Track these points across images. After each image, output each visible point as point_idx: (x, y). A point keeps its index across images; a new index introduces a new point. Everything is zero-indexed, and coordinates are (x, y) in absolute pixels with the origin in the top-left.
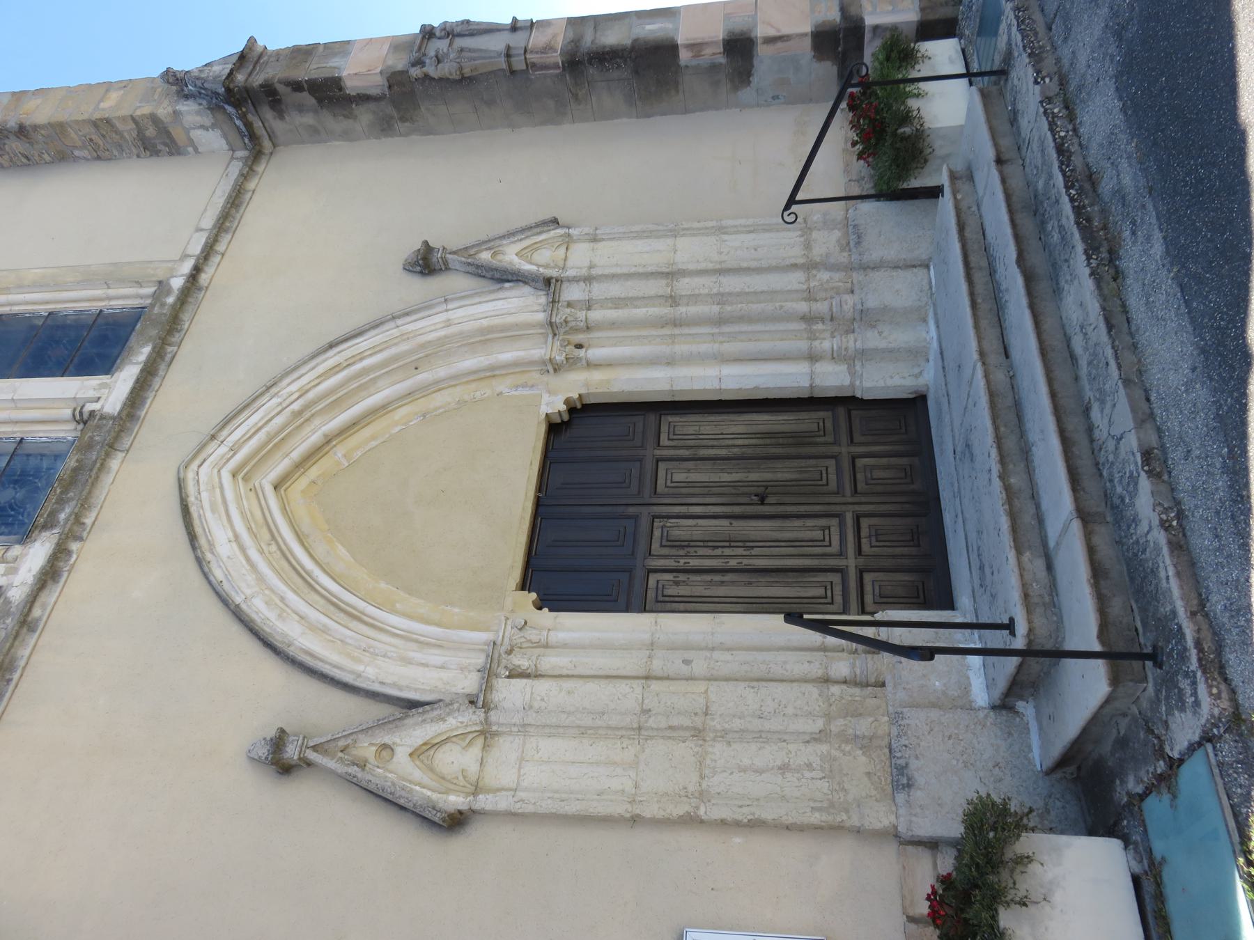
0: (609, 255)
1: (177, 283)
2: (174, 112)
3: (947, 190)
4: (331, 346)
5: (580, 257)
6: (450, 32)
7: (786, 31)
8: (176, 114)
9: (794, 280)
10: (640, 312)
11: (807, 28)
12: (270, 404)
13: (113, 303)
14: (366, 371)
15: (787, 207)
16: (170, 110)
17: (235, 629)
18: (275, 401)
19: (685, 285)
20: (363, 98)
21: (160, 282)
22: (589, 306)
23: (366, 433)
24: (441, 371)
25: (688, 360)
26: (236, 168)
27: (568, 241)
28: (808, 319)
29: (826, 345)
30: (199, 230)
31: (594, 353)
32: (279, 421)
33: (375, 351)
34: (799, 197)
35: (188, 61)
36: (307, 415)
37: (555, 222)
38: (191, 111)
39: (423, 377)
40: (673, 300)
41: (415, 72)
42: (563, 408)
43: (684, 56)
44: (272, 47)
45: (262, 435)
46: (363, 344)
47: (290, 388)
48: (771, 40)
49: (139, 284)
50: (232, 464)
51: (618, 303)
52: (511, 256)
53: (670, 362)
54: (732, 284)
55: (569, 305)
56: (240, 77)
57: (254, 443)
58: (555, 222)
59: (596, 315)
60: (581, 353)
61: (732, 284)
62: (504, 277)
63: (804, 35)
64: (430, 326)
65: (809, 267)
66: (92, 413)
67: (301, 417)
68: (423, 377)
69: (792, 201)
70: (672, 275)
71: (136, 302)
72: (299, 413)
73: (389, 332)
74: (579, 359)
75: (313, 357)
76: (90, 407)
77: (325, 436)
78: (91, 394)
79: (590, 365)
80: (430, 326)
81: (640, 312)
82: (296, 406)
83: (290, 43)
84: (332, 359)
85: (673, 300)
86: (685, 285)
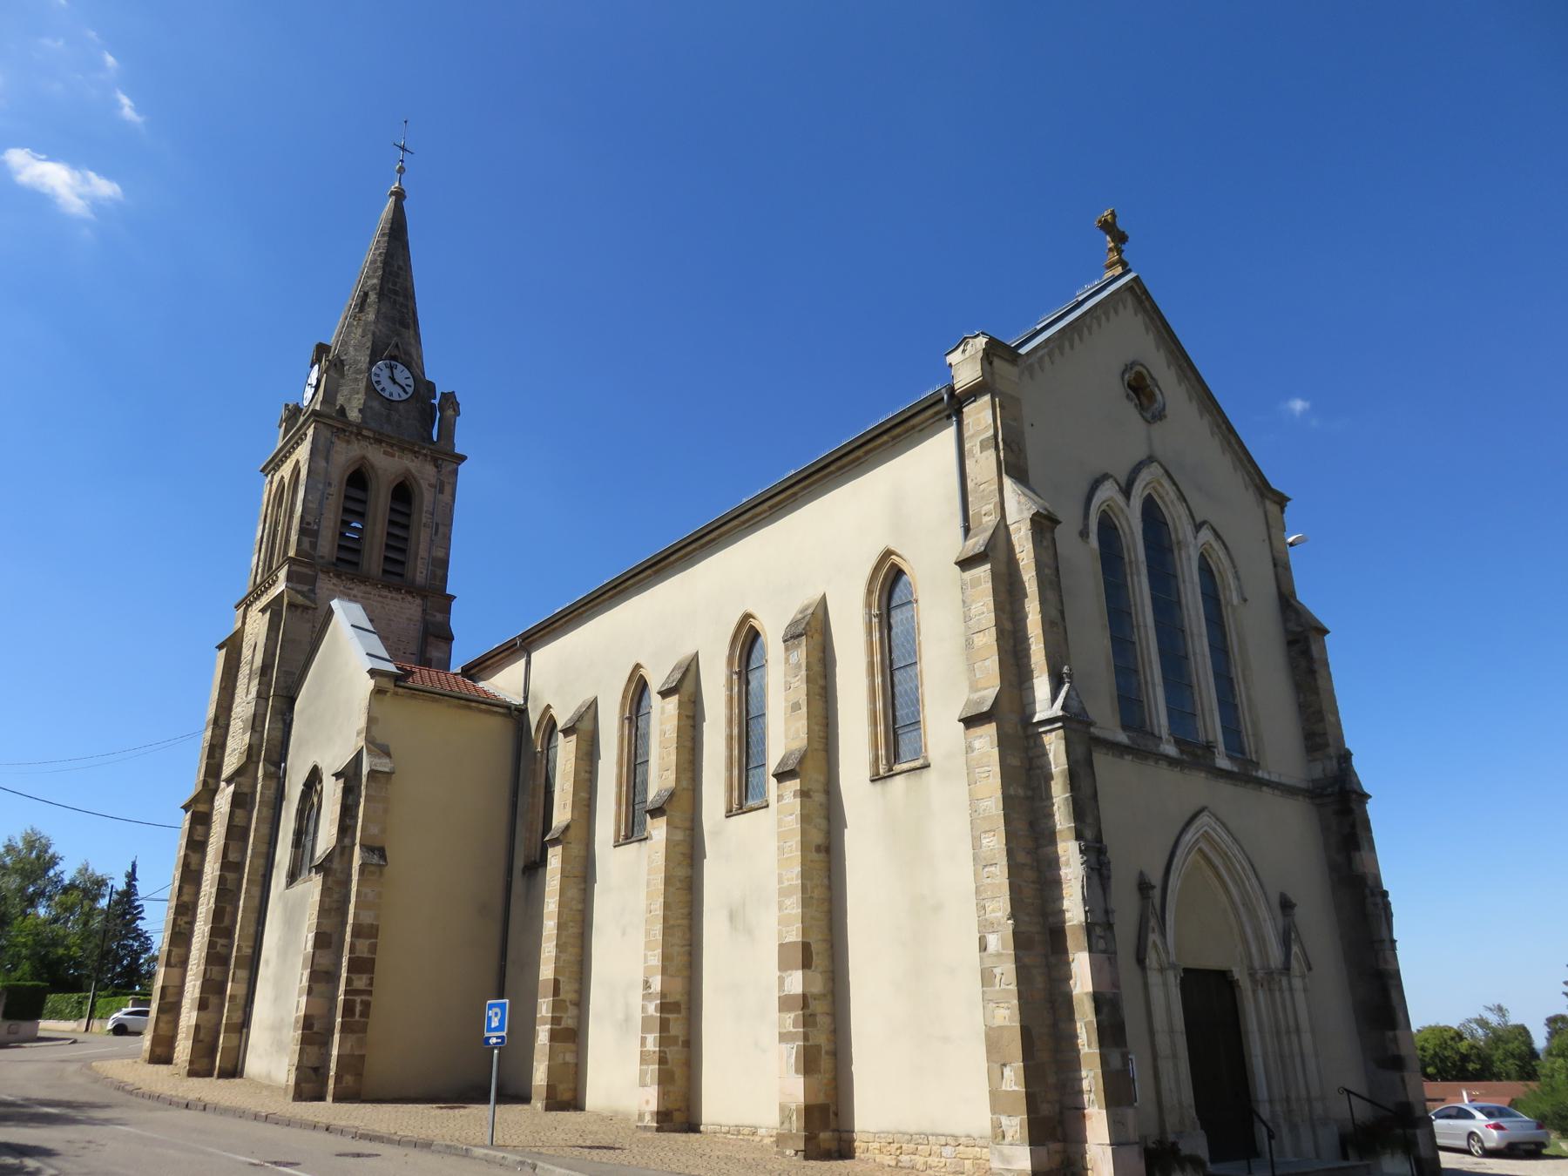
0: (1300, 997)
1: (1260, 774)
2: (1332, 757)
3: (1345, 1164)
4: (1252, 866)
5: (1297, 983)
6: (1387, 906)
7: (1408, 1087)
8: (1330, 758)
9: (1303, 1092)
10: (1281, 1015)
11: (1411, 1098)
12: (1229, 840)
13: (1245, 738)
14: (1243, 882)
15: (1346, 1090)
16: (1332, 754)
17: (1169, 848)
18: (1231, 843)
19: (1294, 1037)
20: (1350, 860)
21: (1258, 764)
22: (1281, 990)
23: (1217, 884)
24: (1245, 918)
25: (1262, 1038)
26: (1303, 785)
27: (1303, 977)
28: (1288, 1099)
29: (1278, 1108)
30: (1280, 775)
31: (1260, 993)
32: (1224, 846)
33: (1252, 887)
34: (638, 761)
35: (1358, 764)
36: (1225, 858)
37: (1310, 969)
38: (1333, 765)
39: (1242, 909)
40: (1288, 1032)
41: (1367, 892)
42: (1236, 978)
43: (1390, 1034)
44: (1368, 807)
45: (1219, 840)
46: (1254, 880)
47: (1235, 849)
48: (1403, 1080)
49: (1256, 752)
50: (1211, 831)
51: (1283, 1001)
52: (1295, 949)
53: (1261, 1030)
54: (1298, 1060)
55: (1280, 980)
56: (1354, 796)
57: (1216, 837)
58: (1310, 969)
59: (1277, 994)
60: (1260, 987)
61: (1298, 1060)
62: (1286, 943)
63: (1407, 1096)
64: (1263, 913)
65: (1309, 1100)
66: (1214, 753)
67: (1225, 856)
68: (1242, 909)
69: (1349, 1092)
70: (1298, 1030)
71: (1247, 750)
72: (1226, 854)
73: (1259, 892)
74: (1257, 986)
75: (1248, 858)
76: (1216, 750)
77: (1217, 867)
78: (1220, 749)
79: (1254, 992)
80: (1263, 913)
81: (1281, 1015)
82: (1229, 853)
83: (1370, 817)
84: (1247, 866)
85: (1288, 1032)
86: (1294, 1037)
